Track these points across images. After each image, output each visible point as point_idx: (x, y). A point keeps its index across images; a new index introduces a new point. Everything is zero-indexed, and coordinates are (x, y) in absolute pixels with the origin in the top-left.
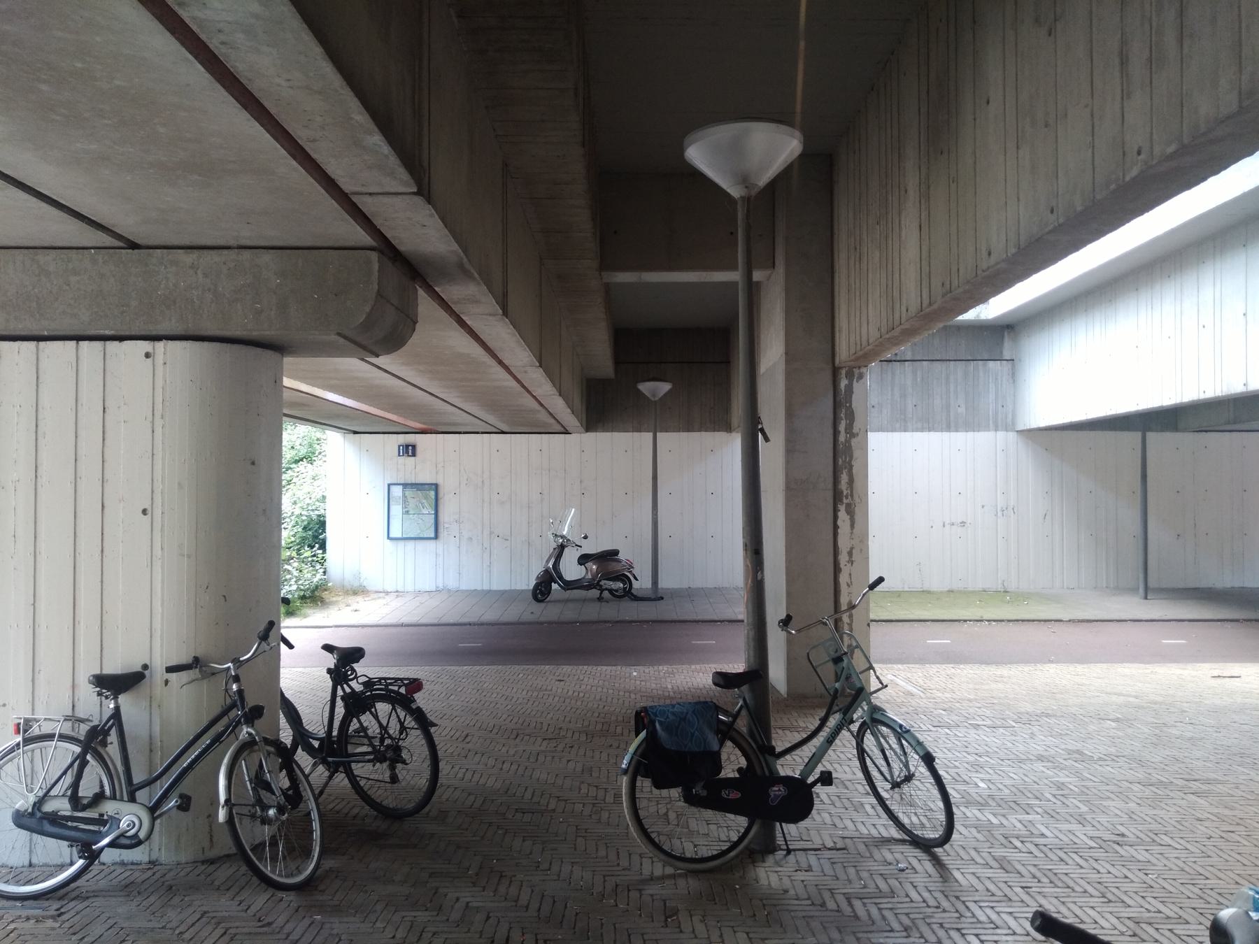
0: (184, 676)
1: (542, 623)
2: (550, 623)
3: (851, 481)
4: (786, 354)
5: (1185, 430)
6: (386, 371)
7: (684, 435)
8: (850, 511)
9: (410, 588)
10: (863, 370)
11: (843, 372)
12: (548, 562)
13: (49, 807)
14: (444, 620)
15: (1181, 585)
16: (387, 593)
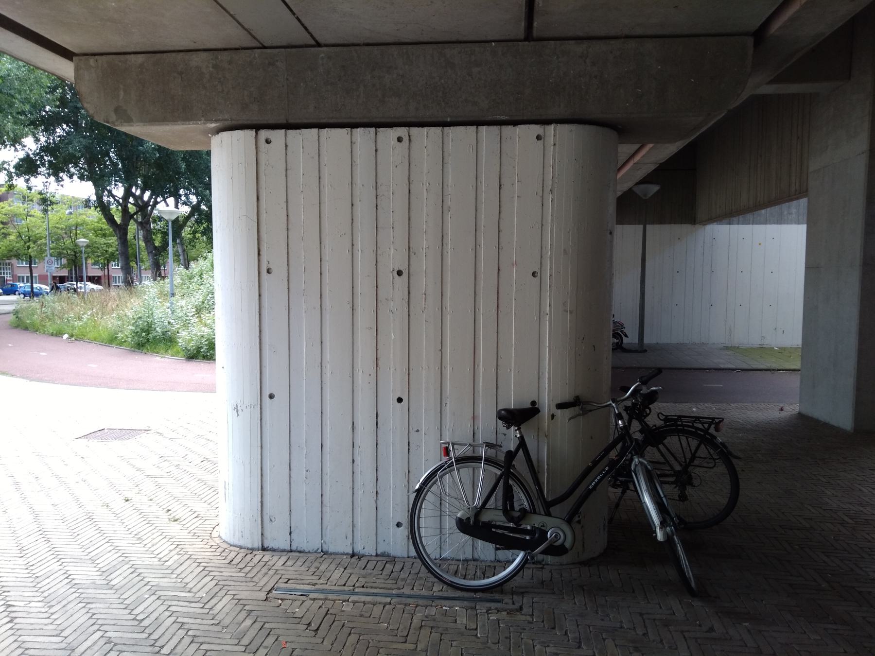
0: (568, 413)
4: (871, 150)
13: (486, 517)
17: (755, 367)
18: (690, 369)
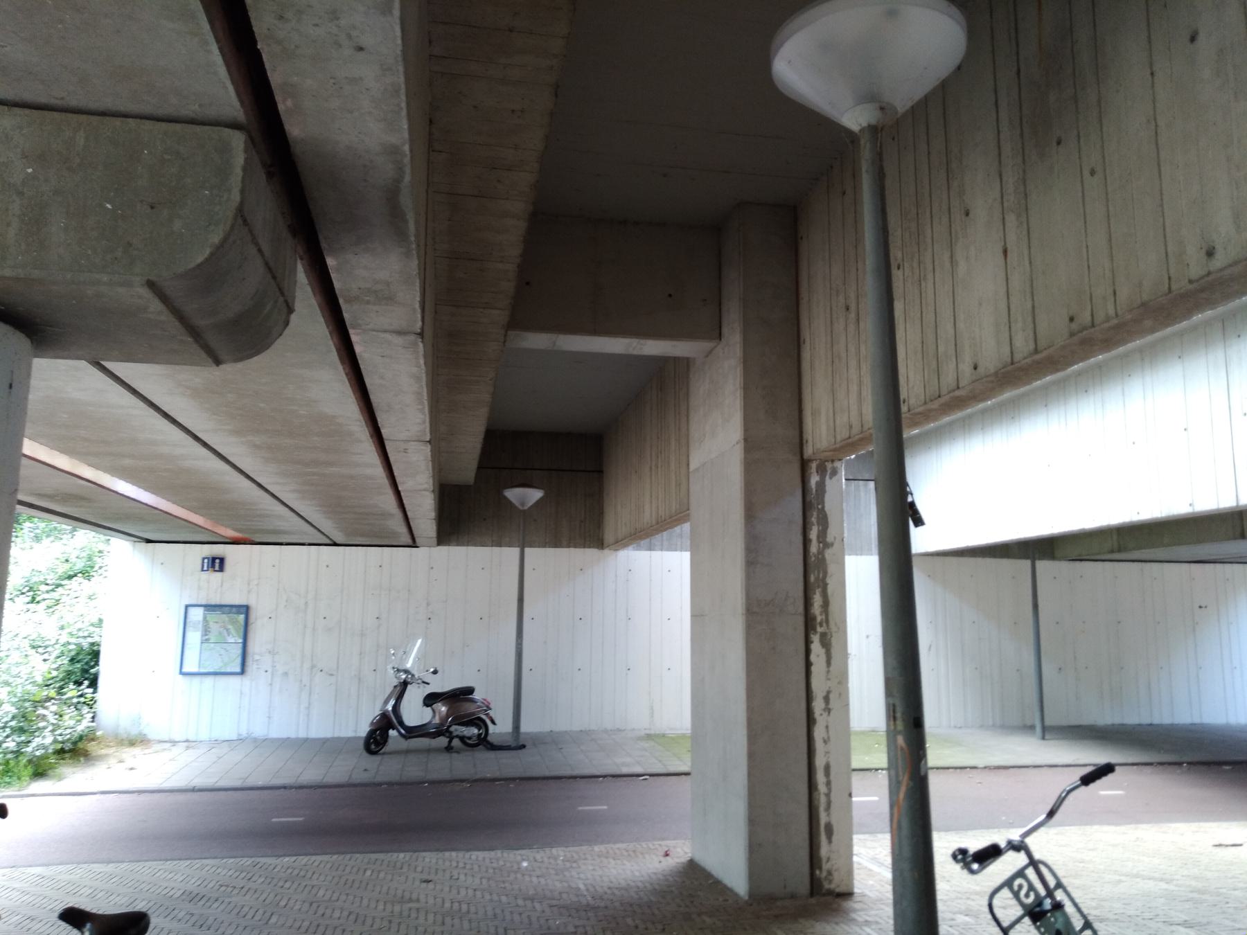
1: (380, 784)
2: (390, 784)
3: (826, 604)
4: (746, 440)
5: (1059, 559)
6: (205, 445)
7: (551, 552)
8: (826, 644)
9: (204, 736)
10: (837, 464)
11: (814, 465)
12: (386, 702)
14: (251, 782)
15: (1064, 723)
16: (174, 743)
17: (672, 769)
18: (574, 777)
